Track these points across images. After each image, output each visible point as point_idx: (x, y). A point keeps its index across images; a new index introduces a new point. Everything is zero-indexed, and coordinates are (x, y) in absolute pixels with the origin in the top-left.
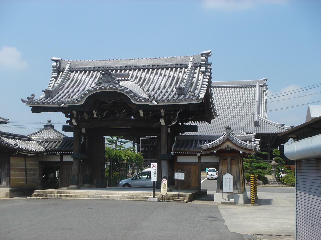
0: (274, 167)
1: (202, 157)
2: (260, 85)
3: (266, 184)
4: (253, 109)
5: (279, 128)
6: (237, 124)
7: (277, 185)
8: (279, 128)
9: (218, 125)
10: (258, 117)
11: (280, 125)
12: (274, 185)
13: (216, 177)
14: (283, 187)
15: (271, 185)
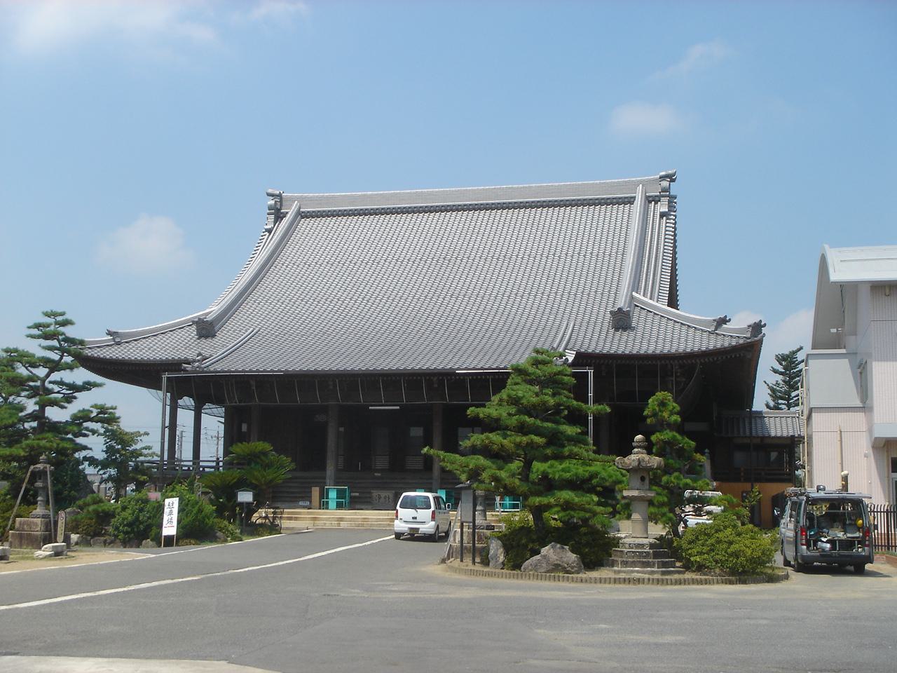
0: (643, 479)
1: (632, 502)
2: (649, 197)
3: (602, 565)
4: (616, 274)
5: (705, 334)
6: (550, 323)
7: (652, 573)
8: (705, 334)
9: (478, 328)
10: (632, 297)
11: (709, 321)
12: (637, 572)
13: (432, 531)
14: (685, 582)
15: (619, 572)
